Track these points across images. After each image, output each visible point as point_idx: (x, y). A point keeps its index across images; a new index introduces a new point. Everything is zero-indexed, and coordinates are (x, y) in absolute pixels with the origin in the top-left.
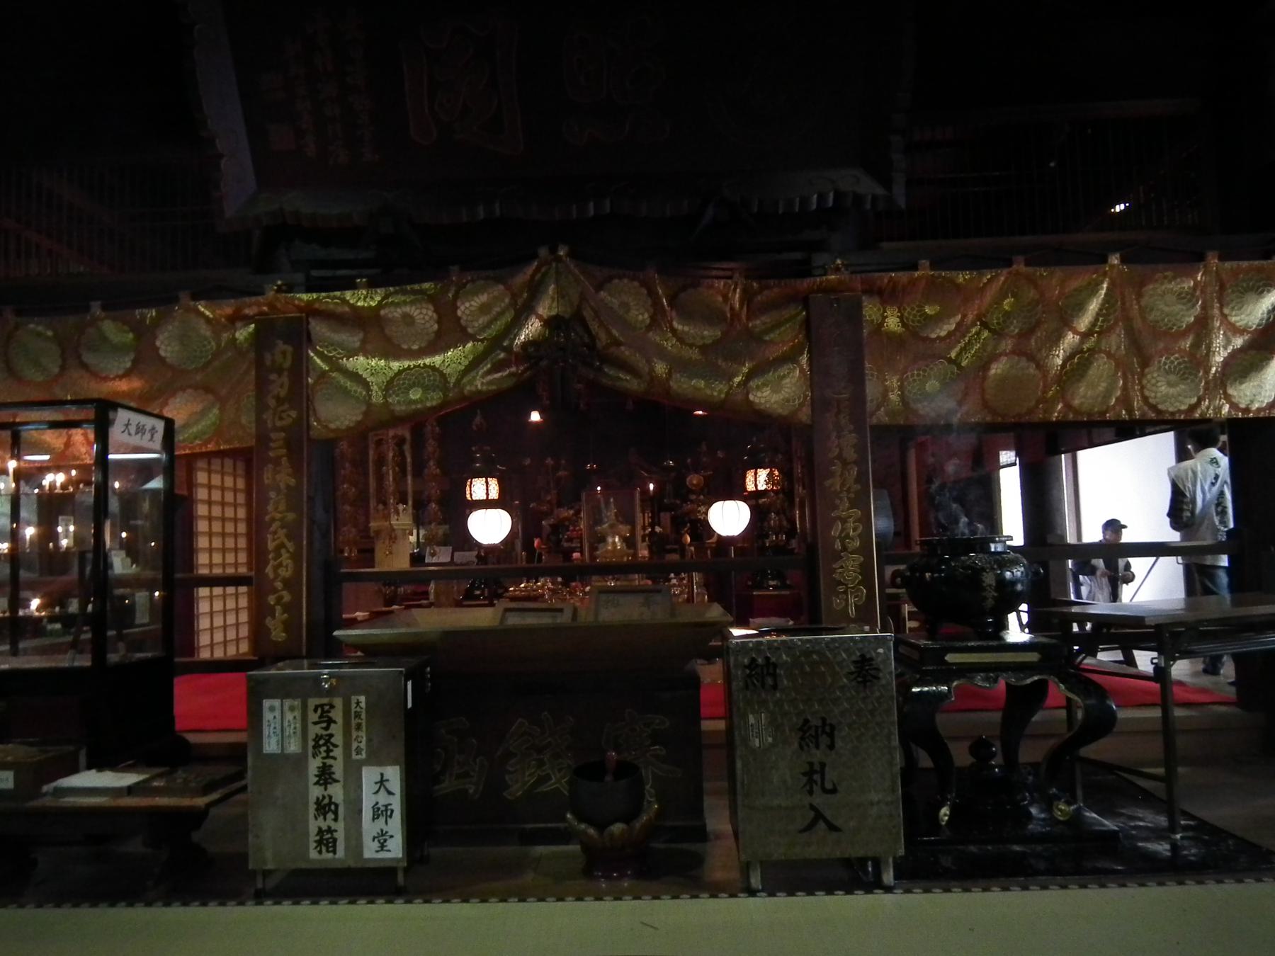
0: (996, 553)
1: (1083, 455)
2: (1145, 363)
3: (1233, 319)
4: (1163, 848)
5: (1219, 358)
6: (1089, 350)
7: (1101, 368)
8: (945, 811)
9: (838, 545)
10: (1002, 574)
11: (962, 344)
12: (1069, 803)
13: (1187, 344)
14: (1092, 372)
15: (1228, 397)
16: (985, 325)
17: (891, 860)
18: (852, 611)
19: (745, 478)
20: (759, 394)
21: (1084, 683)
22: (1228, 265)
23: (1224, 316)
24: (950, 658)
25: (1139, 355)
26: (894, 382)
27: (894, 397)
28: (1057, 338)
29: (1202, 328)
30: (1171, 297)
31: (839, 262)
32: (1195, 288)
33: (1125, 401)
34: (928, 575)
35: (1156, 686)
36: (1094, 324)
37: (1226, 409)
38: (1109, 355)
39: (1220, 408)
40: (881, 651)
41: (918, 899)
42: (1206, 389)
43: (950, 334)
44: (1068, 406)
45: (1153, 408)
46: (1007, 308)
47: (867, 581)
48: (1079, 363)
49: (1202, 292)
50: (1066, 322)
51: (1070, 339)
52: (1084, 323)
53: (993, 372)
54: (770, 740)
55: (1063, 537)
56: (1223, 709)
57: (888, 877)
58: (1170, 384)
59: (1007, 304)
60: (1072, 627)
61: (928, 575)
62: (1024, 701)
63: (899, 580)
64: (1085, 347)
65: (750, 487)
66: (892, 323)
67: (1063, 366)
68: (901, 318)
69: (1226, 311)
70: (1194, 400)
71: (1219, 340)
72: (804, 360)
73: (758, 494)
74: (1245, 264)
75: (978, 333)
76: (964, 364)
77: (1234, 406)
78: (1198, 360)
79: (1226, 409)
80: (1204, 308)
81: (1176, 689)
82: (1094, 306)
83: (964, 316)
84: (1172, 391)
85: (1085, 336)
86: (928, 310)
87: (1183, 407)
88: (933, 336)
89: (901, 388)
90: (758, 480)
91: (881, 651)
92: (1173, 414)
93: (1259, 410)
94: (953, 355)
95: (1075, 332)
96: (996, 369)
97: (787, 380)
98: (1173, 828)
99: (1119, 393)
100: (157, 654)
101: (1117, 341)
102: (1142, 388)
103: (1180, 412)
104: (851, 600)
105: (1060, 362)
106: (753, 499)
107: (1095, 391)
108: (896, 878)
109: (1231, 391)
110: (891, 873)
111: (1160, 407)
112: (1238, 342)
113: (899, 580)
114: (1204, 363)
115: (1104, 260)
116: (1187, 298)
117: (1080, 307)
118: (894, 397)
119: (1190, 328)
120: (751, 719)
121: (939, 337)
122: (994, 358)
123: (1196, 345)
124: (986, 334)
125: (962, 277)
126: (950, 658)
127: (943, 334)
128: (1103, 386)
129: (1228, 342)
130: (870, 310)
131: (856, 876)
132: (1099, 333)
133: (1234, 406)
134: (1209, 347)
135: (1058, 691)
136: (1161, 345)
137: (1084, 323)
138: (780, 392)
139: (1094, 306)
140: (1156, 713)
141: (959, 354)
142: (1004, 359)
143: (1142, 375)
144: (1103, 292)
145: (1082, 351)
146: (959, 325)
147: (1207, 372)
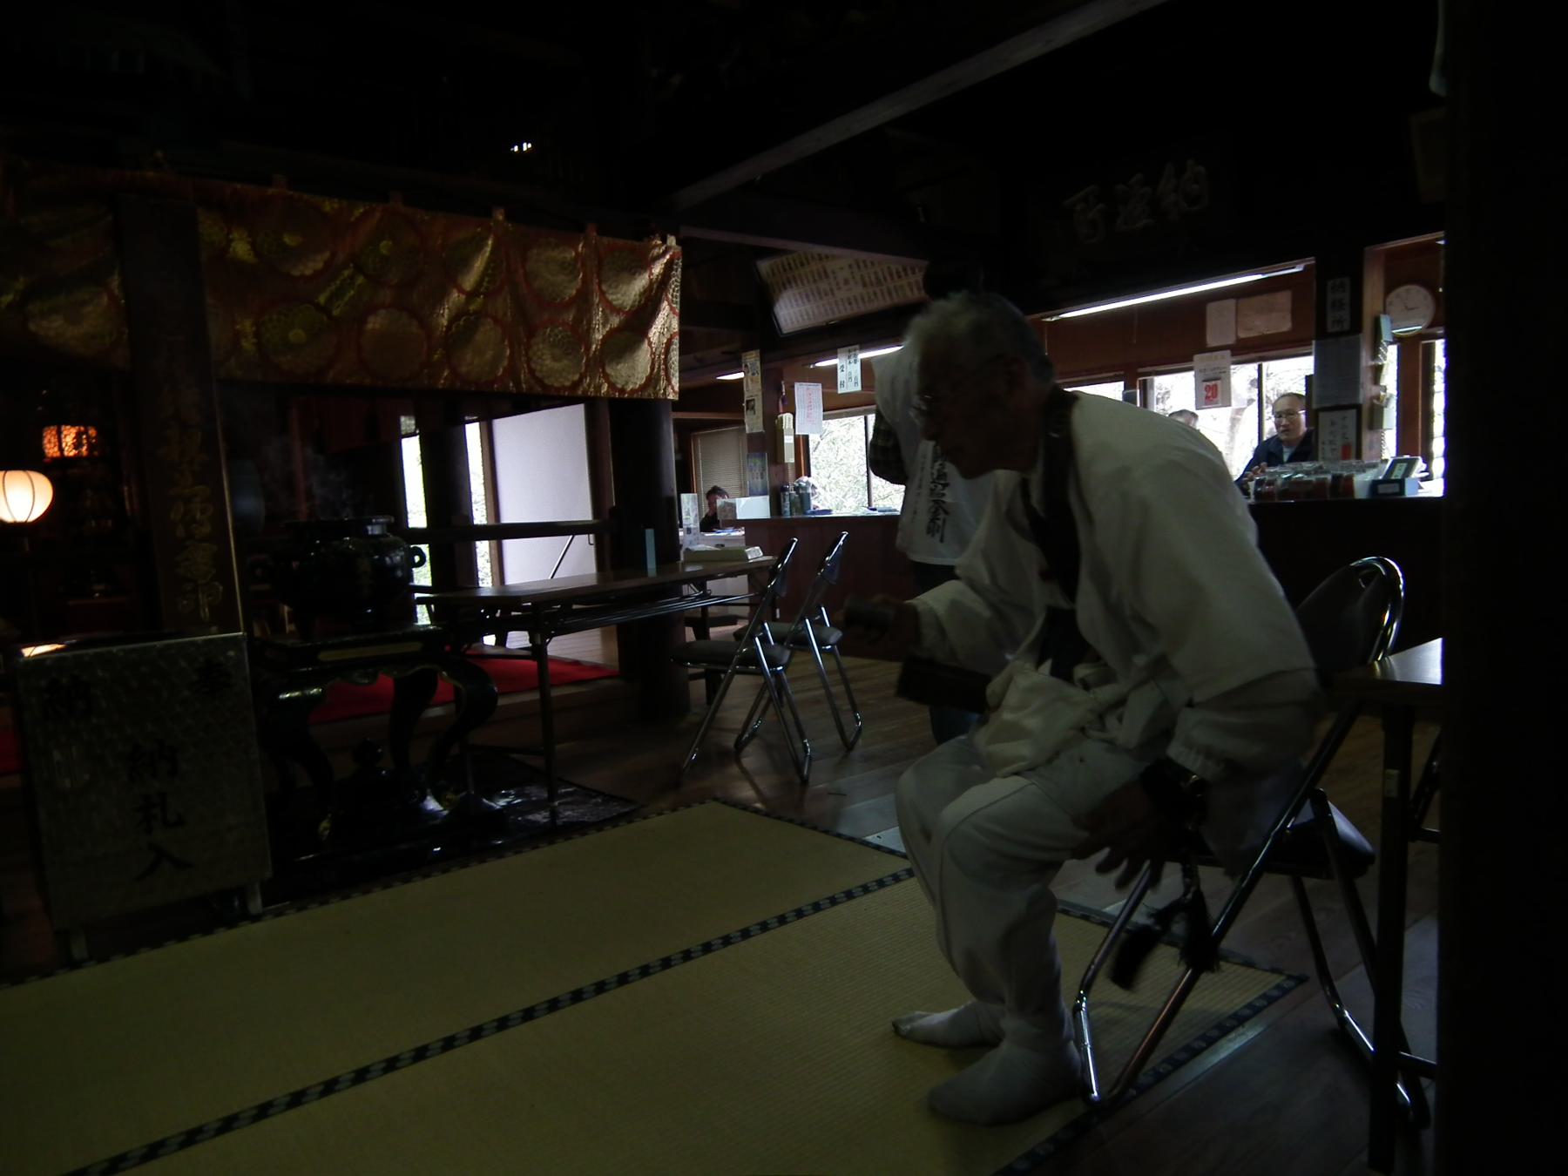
0: (374, 536)
1: (502, 426)
2: (531, 333)
3: (610, 297)
4: (541, 817)
5: (598, 336)
6: (475, 312)
7: (487, 334)
8: (325, 824)
9: (180, 532)
10: (382, 560)
11: (333, 287)
12: (456, 792)
13: (570, 317)
14: (480, 337)
15: (607, 377)
16: (359, 269)
17: (257, 886)
18: (206, 612)
19: (41, 438)
20: (45, 323)
21: (477, 669)
22: (605, 240)
23: (603, 293)
24: (324, 656)
25: (523, 329)
26: (247, 325)
27: (248, 345)
28: (440, 296)
29: (583, 302)
30: (555, 265)
31: (159, 154)
32: (576, 259)
33: (512, 371)
34: (295, 564)
35: (533, 664)
36: (479, 283)
37: (605, 388)
38: (496, 321)
39: (599, 387)
40: (231, 653)
41: (293, 922)
42: (587, 365)
43: (317, 274)
44: (454, 371)
45: (540, 381)
46: (384, 251)
47: (224, 574)
48: (466, 323)
49: (583, 265)
50: (450, 277)
51: (455, 297)
52: (469, 281)
53: (370, 326)
54: (87, 777)
55: (469, 517)
56: (607, 682)
57: (256, 905)
58: (555, 359)
59: (385, 246)
60: (413, 616)
61: (295, 564)
62: (416, 691)
63: (259, 572)
64: (472, 308)
65: (51, 450)
66: (241, 248)
67: (449, 327)
68: (253, 245)
69: (604, 288)
70: (576, 377)
71: (598, 317)
72: (115, 282)
73: (62, 460)
74: (620, 242)
75: (352, 278)
76: (335, 313)
77: (612, 386)
78: (581, 334)
79: (605, 388)
80: (584, 281)
81: (551, 666)
82: (479, 264)
83: (333, 255)
84: (557, 365)
85: (472, 295)
86: (287, 239)
87: (568, 384)
88: (296, 273)
89: (257, 335)
90: (66, 441)
91: (231, 653)
92: (558, 389)
93: (633, 391)
94: (322, 299)
95: (461, 291)
96: (374, 323)
97: (89, 309)
98: (552, 798)
99: (505, 363)
100: (1367, 846)
101: (503, 305)
102: (529, 361)
103: (565, 388)
104: (203, 599)
105: (445, 322)
106: (56, 470)
107: (484, 355)
108: (265, 904)
109: (609, 370)
110: (259, 901)
111: (546, 381)
112: (615, 321)
113: (259, 572)
114: (584, 337)
115: (488, 214)
116: (569, 268)
117: (466, 263)
118: (248, 345)
119: (573, 300)
120: (57, 756)
121: (302, 276)
122: (372, 309)
123: (578, 320)
124: (360, 280)
125: (328, 206)
126: (324, 656)
127: (308, 272)
128: (489, 355)
129: (606, 321)
130: (210, 228)
131: (218, 911)
132: (486, 295)
133: (612, 386)
134: (589, 322)
135: (445, 683)
136: (546, 316)
137: (469, 281)
138: (80, 323)
139: (479, 264)
140: (536, 696)
141: (330, 300)
142: (382, 312)
143: (528, 347)
144: (488, 249)
145: (467, 313)
146: (327, 264)
147: (588, 348)
